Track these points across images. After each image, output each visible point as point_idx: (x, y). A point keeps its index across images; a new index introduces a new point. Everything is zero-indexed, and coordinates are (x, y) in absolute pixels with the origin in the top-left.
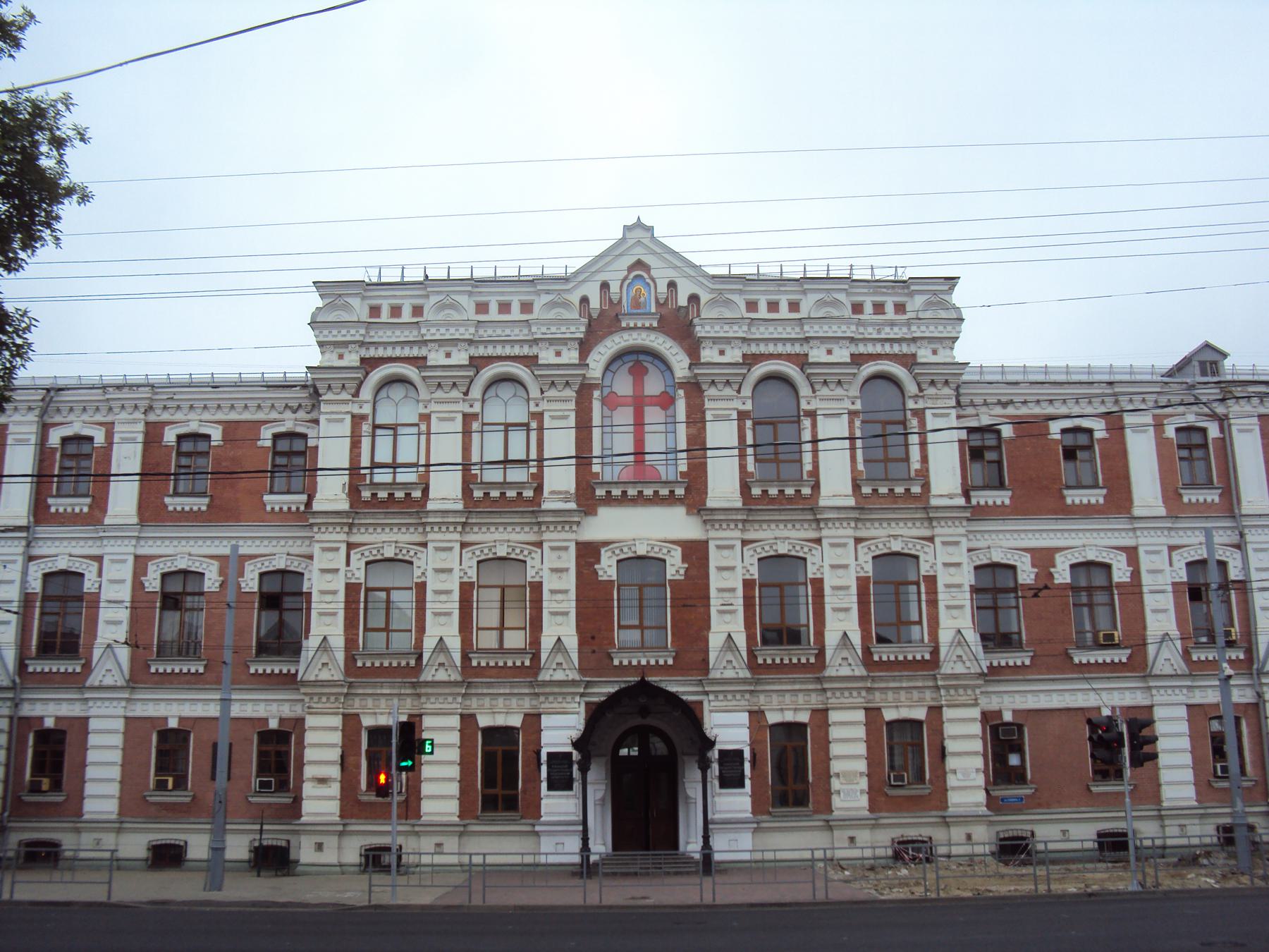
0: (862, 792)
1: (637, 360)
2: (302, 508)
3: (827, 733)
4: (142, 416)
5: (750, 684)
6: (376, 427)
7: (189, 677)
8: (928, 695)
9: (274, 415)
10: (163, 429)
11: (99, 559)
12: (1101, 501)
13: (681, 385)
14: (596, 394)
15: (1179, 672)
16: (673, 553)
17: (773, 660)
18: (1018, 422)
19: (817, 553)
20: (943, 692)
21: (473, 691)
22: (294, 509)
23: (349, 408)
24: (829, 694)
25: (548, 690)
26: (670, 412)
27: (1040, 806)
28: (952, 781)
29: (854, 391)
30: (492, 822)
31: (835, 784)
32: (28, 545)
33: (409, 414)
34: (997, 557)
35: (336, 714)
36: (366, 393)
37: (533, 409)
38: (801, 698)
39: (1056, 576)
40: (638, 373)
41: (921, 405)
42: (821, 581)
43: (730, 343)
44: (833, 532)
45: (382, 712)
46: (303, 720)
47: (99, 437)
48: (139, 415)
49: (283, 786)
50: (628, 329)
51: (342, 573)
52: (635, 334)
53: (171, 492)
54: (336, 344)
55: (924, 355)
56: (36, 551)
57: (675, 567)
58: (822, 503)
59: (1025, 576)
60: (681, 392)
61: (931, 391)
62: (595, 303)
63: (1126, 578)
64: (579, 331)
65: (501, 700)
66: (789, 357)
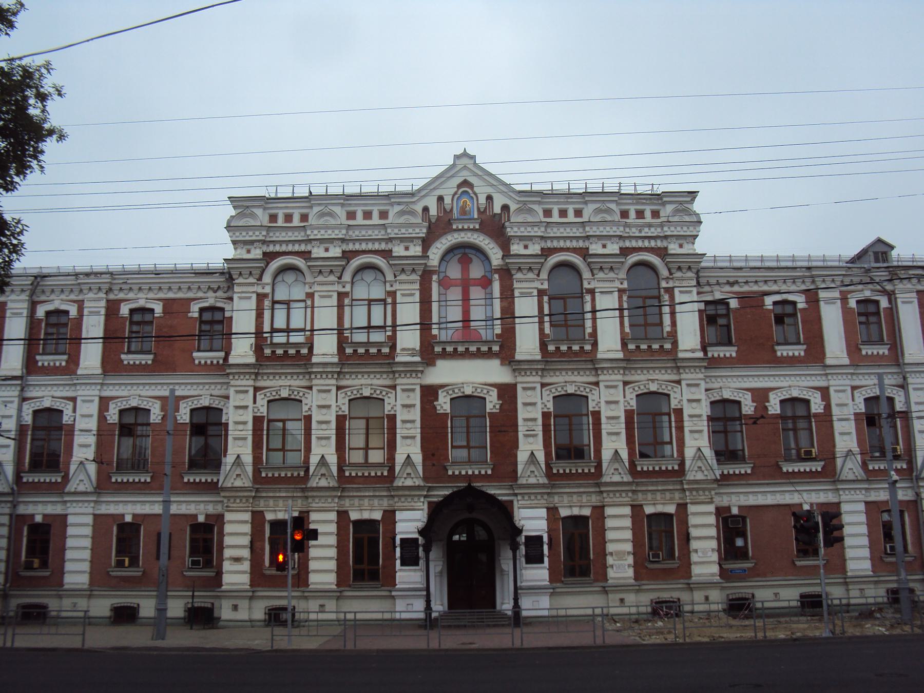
0: (629, 566)
2: (221, 362)
4: (104, 296)
5: (548, 488)
6: (274, 302)
7: (139, 485)
8: (677, 495)
9: (200, 294)
11: (74, 400)
12: (802, 354)
13: (496, 271)
14: (435, 277)
15: (859, 478)
17: (564, 471)
18: (742, 297)
20: (687, 493)
21: (346, 494)
22: (215, 362)
24: (605, 495)
25: (400, 493)
26: (488, 290)
27: (758, 576)
28: (694, 558)
29: (622, 275)
30: (361, 589)
31: (610, 560)
32: (22, 390)
33: (298, 292)
34: (727, 395)
36: (267, 278)
37: (389, 288)
39: (770, 408)
40: (465, 262)
41: (671, 285)
42: (599, 413)
43: (531, 240)
44: (405, 381)
45: (280, 510)
46: (222, 516)
47: (73, 311)
48: (102, 295)
49: (208, 564)
51: (250, 409)
52: (462, 234)
53: (126, 350)
54: (246, 243)
55: (673, 248)
56: (28, 394)
57: (492, 403)
59: (747, 409)
60: (496, 276)
61: (678, 274)
62: (433, 211)
63: (820, 410)
64: (422, 232)
65: (366, 500)
66: (575, 250)
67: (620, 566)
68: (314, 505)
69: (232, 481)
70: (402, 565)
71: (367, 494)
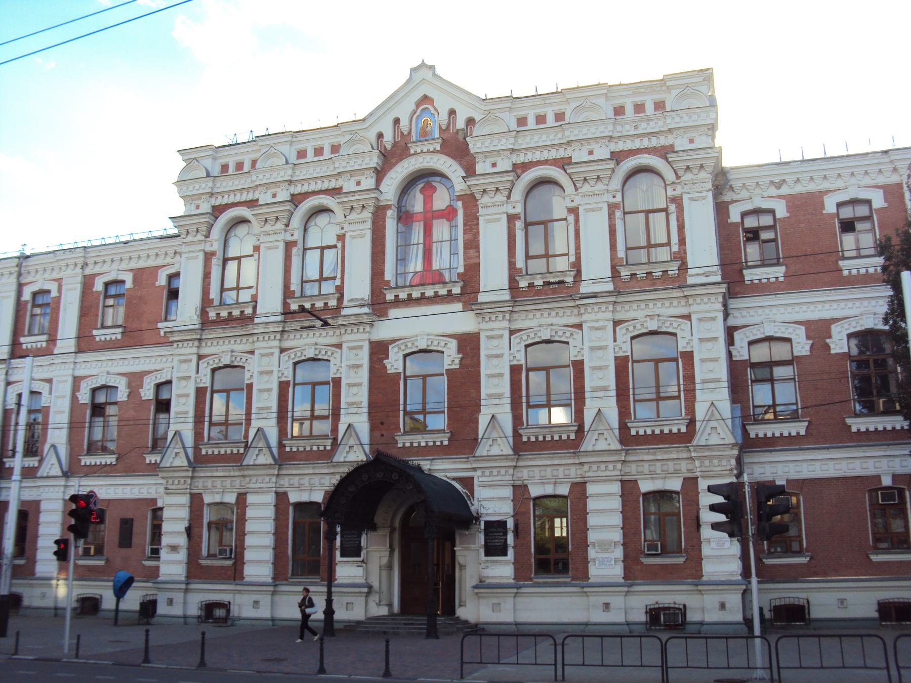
1: (424, 178)
3: (585, 505)
5: (512, 460)
8: (684, 466)
9: (840, 184)
10: (94, 279)
11: (49, 381)
13: (459, 198)
16: (449, 345)
19: (337, 355)
21: (284, 472)
23: (201, 247)
26: (453, 223)
27: (816, 574)
31: (592, 553)
32: (7, 374)
35: (185, 493)
36: (217, 232)
37: (670, 192)
38: (316, 480)
39: (832, 346)
41: (679, 191)
42: (581, 362)
43: (200, 199)
44: (703, 307)
47: (53, 287)
50: (416, 154)
51: (193, 379)
53: (99, 326)
55: (681, 143)
57: (451, 358)
58: (690, 281)
61: (688, 176)
62: (388, 138)
64: (374, 160)
66: (555, 162)
67: (605, 561)
68: (251, 485)
69: (705, 436)
70: (342, 556)
71: (306, 472)
